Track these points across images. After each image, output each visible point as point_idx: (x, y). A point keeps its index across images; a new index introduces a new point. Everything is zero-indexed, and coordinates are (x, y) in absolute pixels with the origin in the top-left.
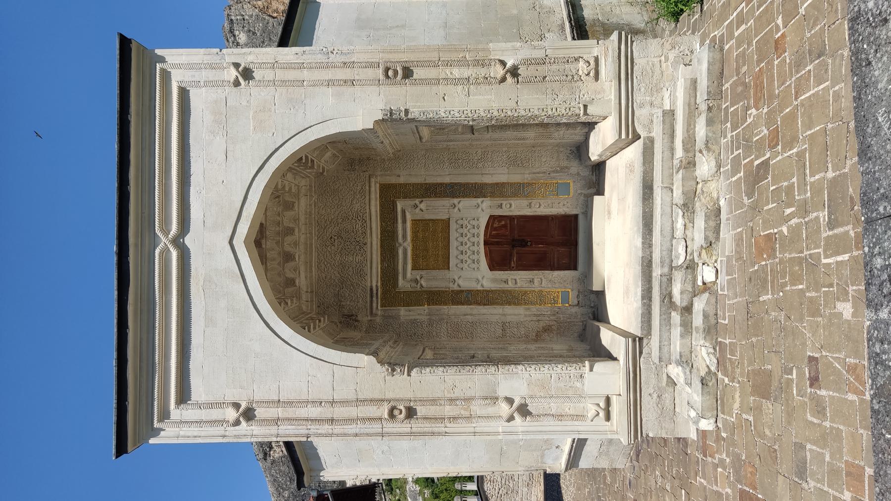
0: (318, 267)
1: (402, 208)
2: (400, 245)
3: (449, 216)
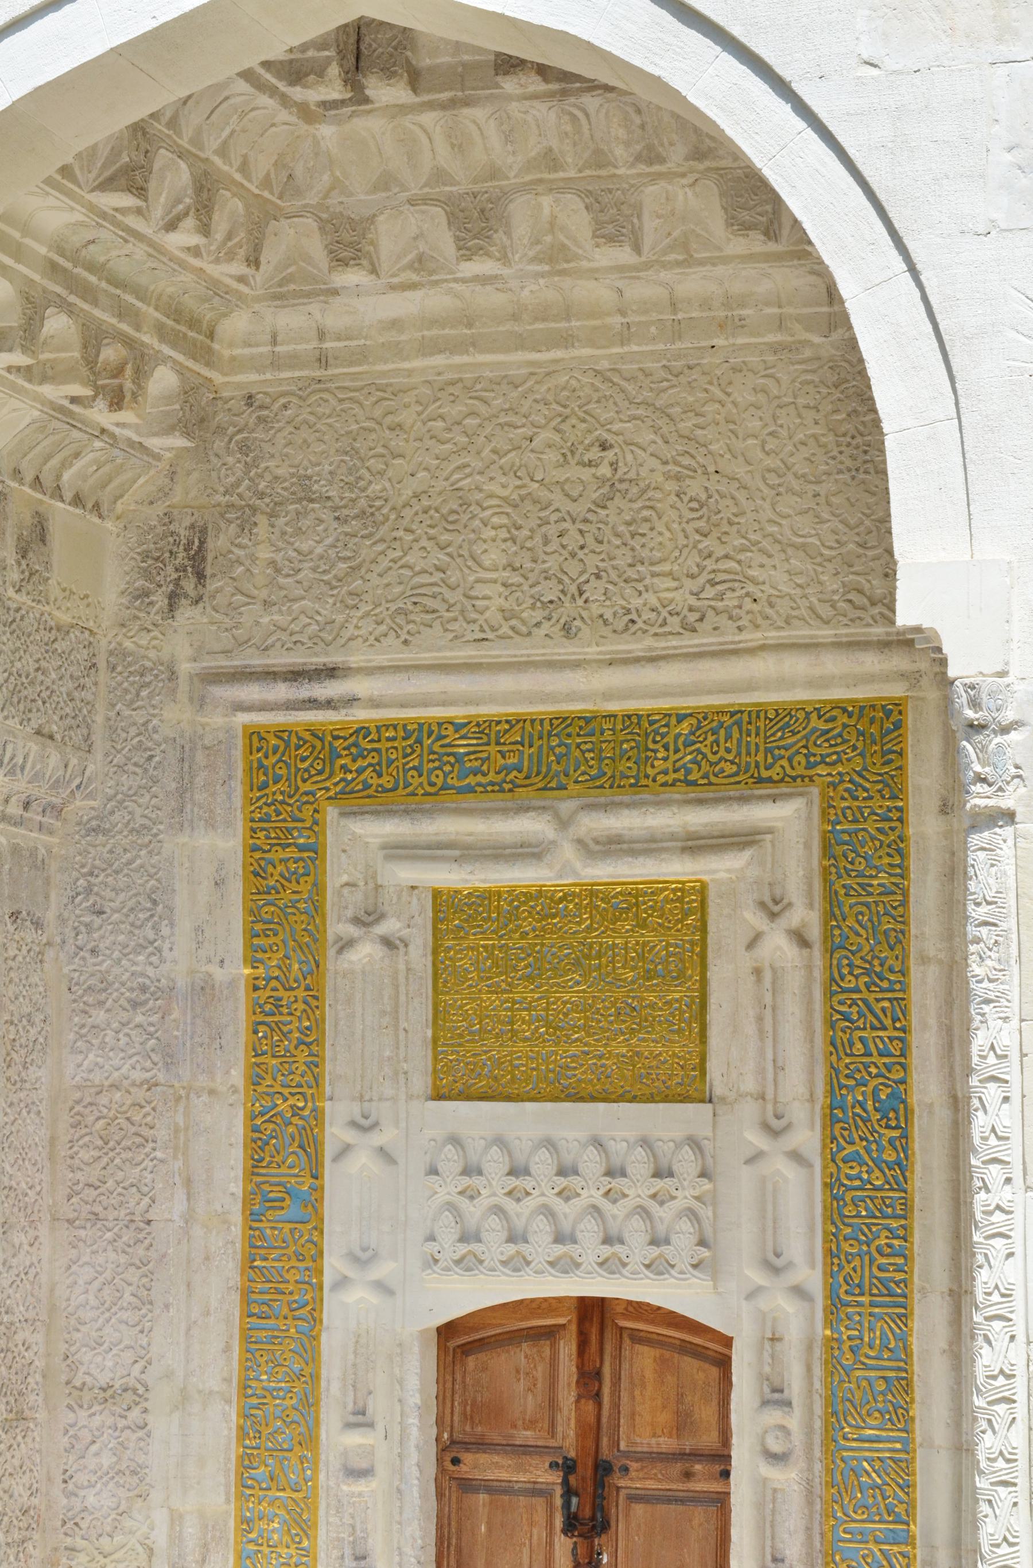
0: (452, 383)
1: (770, 831)
2: (563, 824)
3: (723, 1099)
